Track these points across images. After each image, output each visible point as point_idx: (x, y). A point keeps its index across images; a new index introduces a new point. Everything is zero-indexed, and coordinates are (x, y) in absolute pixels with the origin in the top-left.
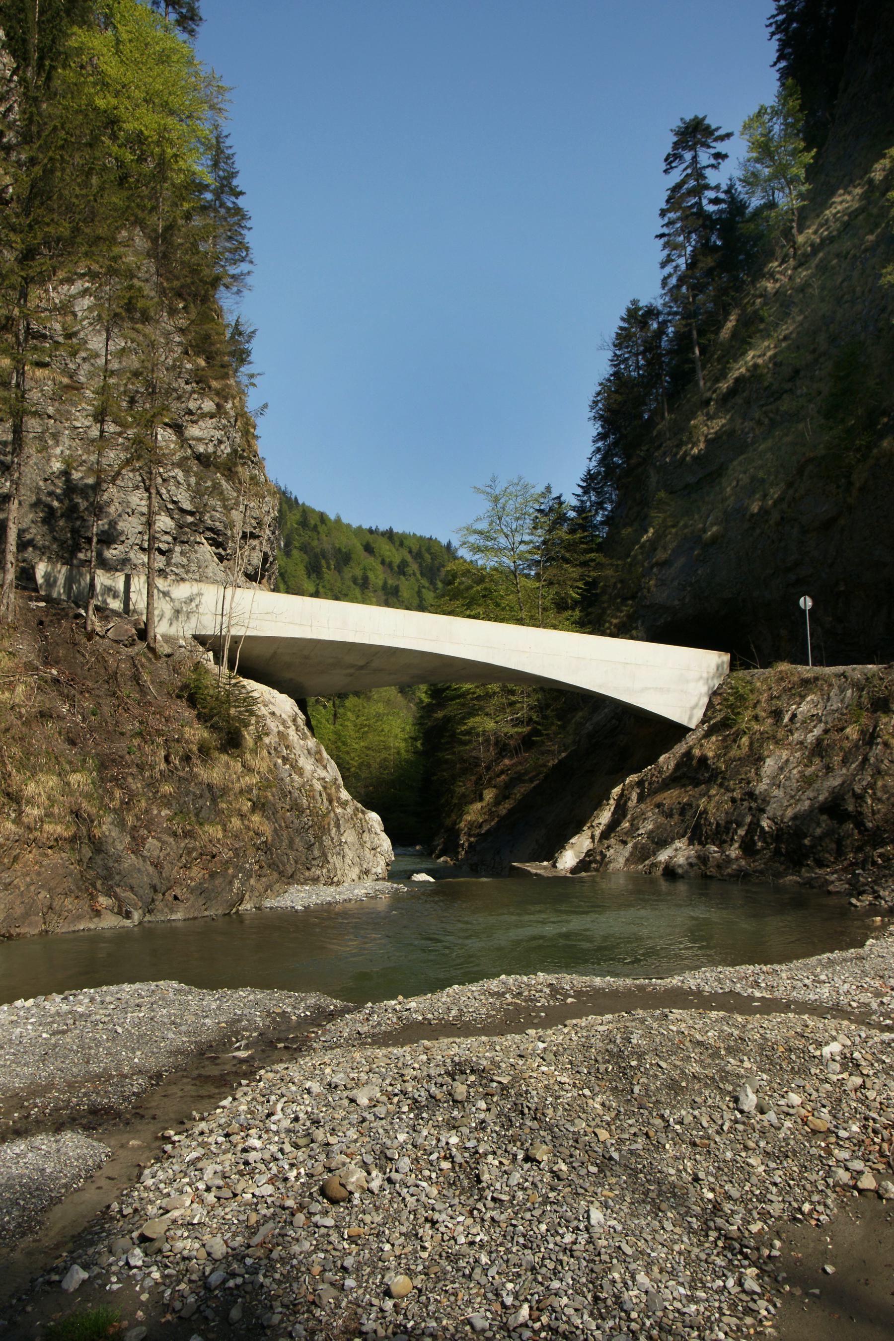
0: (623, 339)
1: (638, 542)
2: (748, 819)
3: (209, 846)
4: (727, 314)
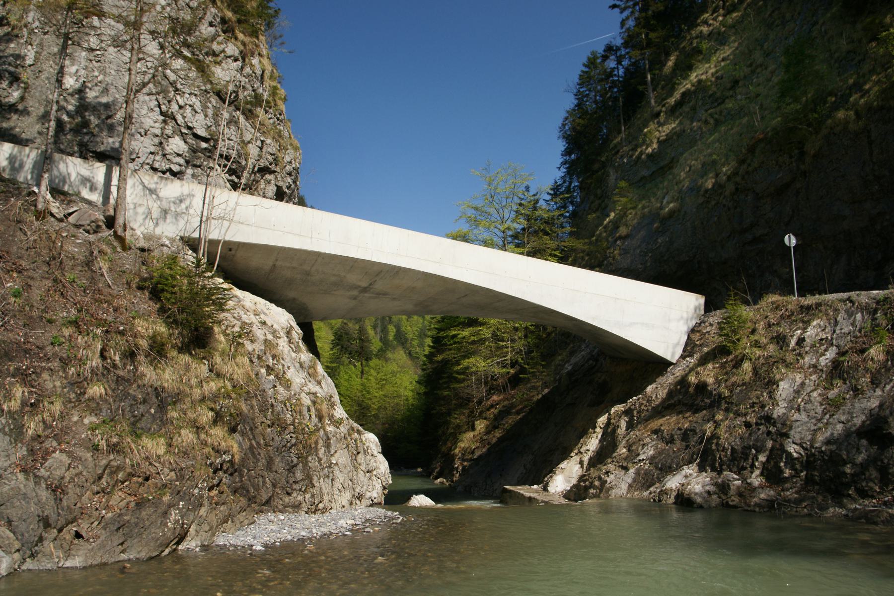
0: (585, 79)
1: (601, 224)
2: (769, 444)
3: (145, 465)
4: (668, 55)
